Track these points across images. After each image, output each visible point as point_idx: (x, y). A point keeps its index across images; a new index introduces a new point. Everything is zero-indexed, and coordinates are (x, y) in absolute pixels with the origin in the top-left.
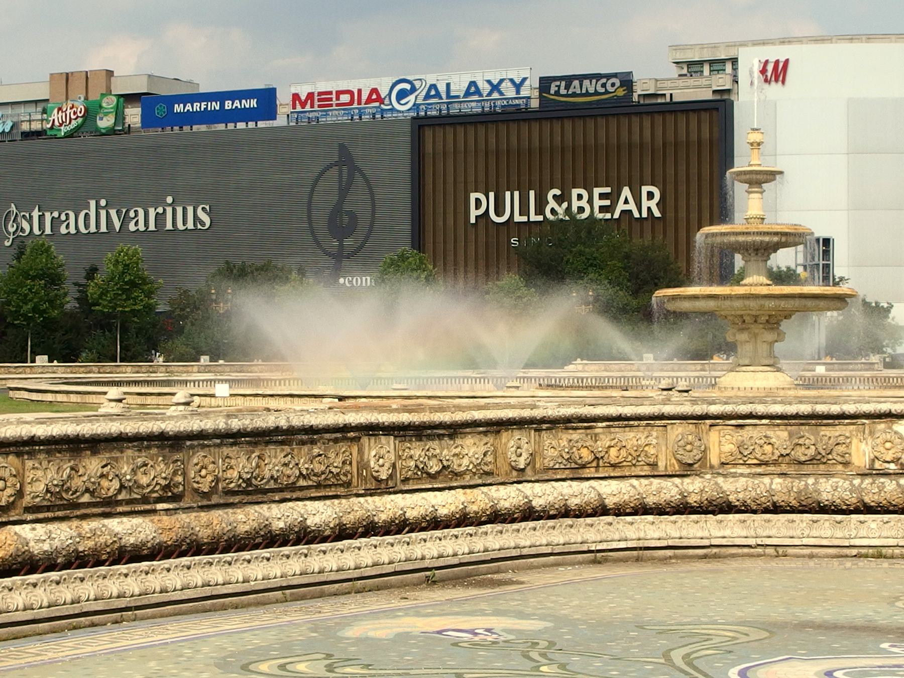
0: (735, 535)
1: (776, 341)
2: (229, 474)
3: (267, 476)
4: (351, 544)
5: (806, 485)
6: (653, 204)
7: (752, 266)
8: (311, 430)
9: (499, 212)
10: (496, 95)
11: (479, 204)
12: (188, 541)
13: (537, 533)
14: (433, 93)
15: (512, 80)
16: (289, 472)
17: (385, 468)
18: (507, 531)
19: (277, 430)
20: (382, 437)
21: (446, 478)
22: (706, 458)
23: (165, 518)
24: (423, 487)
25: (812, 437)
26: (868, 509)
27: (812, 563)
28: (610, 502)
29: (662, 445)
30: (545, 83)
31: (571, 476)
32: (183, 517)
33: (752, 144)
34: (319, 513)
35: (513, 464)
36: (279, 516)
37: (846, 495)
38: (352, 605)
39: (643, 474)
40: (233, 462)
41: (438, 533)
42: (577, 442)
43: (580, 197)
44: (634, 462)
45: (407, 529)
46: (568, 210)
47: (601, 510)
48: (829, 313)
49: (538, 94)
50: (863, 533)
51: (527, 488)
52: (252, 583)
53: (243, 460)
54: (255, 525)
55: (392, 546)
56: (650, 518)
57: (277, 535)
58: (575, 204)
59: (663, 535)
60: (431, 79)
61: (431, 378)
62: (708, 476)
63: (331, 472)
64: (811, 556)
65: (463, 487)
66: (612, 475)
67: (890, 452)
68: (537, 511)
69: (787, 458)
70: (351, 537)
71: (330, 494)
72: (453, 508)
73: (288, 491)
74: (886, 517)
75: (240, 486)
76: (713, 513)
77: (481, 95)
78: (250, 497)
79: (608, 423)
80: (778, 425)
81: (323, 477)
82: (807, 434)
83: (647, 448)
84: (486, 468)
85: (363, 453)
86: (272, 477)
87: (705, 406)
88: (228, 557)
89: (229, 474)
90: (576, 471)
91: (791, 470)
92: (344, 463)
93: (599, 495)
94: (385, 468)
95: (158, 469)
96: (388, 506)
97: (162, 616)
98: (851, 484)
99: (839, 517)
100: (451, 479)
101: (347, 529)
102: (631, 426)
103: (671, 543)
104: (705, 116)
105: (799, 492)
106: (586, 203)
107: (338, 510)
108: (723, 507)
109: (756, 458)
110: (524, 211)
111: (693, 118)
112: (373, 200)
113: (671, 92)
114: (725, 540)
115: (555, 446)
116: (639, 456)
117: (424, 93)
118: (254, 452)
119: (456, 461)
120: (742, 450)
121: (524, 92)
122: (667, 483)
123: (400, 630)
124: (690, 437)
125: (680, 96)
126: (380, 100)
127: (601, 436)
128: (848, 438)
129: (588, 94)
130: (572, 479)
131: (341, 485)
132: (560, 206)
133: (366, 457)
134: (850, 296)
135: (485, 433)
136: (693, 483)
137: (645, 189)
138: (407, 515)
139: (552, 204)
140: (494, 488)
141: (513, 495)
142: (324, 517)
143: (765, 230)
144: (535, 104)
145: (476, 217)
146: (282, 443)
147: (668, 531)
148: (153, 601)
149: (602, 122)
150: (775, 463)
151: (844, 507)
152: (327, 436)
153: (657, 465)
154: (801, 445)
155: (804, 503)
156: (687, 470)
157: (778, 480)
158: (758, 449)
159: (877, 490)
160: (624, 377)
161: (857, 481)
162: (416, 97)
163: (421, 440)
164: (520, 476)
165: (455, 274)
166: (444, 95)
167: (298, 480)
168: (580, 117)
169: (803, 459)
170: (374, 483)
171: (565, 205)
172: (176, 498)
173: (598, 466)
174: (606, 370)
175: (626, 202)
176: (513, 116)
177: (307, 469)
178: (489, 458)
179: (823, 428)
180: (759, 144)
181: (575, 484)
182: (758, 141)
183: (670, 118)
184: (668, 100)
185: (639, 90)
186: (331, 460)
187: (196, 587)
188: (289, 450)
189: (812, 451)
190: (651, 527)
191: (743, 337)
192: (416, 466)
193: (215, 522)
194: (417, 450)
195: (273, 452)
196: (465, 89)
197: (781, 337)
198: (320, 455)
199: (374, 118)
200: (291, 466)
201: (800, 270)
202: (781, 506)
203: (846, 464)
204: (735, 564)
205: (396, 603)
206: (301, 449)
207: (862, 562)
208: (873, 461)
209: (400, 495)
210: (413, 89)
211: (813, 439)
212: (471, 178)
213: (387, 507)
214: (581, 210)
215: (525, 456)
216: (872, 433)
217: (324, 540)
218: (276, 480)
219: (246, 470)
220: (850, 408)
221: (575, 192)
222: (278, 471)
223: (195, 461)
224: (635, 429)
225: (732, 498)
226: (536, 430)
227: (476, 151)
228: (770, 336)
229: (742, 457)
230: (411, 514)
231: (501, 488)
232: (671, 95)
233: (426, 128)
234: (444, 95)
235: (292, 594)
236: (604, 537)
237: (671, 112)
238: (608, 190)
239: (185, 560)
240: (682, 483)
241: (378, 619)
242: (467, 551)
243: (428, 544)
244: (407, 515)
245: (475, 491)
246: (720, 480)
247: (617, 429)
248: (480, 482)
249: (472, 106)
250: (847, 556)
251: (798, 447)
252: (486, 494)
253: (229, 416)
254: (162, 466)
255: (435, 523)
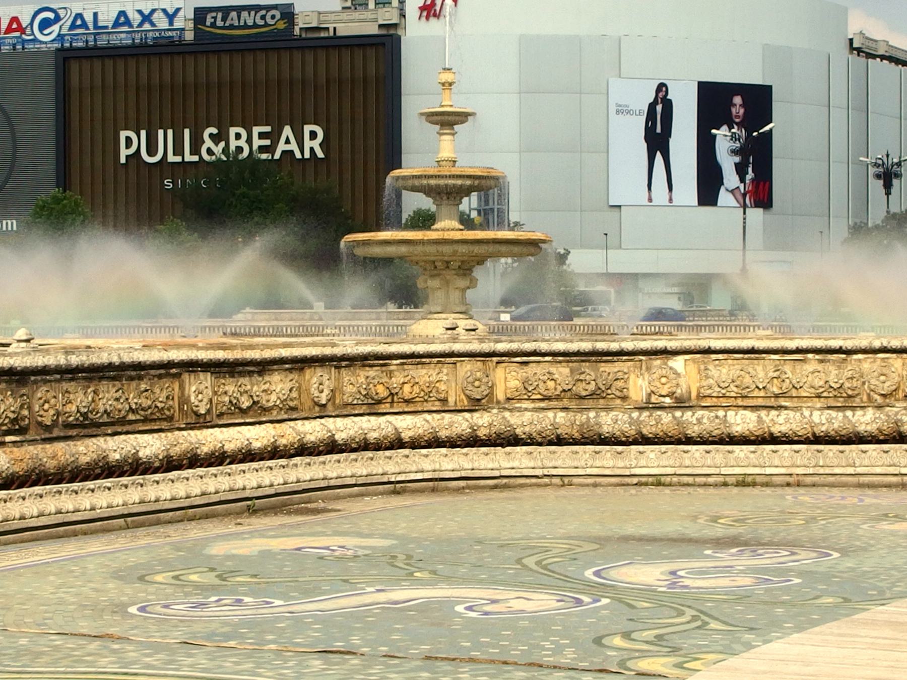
0: (523, 466)
1: (469, 288)
2: (68, 408)
3: (102, 410)
4: (180, 475)
5: (588, 418)
6: (316, 144)
7: (444, 210)
8: (139, 367)
9: (151, 151)
10: (147, 26)
11: (130, 143)
12: (37, 471)
13: (342, 465)
14: (79, 22)
15: (164, 11)
16: (120, 406)
17: (204, 403)
18: (315, 463)
19: (110, 366)
20: (201, 374)
21: (257, 413)
22: (493, 394)
23: (15, 449)
24: (237, 421)
25: (592, 373)
26: (644, 440)
27: (599, 490)
28: (406, 436)
29: (451, 381)
30: (200, 14)
31: (368, 411)
32: (32, 450)
33: (443, 84)
34: (150, 445)
35: (316, 399)
36: (115, 448)
37: (626, 427)
38: (212, 528)
39: (434, 409)
40: (72, 397)
41: (255, 465)
42: (373, 378)
43: (238, 136)
44: (426, 398)
45: (228, 461)
46: (225, 151)
47: (397, 443)
48: (503, 260)
49: (192, 25)
50: (643, 462)
51: (330, 423)
52: (98, 511)
53: (80, 396)
54: (95, 457)
55: (216, 476)
56: (443, 450)
57: (113, 466)
59: (457, 466)
60: (76, 9)
61: (100, 327)
62: (495, 411)
63: (156, 407)
64: (595, 485)
65: (272, 422)
66: (406, 410)
67: (666, 387)
68: (339, 445)
69: (569, 394)
70: (179, 467)
71: (156, 427)
72: (265, 442)
73: (118, 424)
74: (664, 448)
75: (77, 419)
76: (502, 445)
77: (131, 26)
78: (86, 430)
79: (402, 361)
80: (560, 362)
81: (150, 411)
82: (588, 370)
83: (437, 385)
84: (292, 404)
85: (184, 389)
86: (105, 411)
87: (492, 344)
88: (75, 486)
89: (68, 408)
90: (373, 406)
91: (573, 405)
92: (168, 398)
93: (396, 429)
94: (204, 403)
95: (8, 403)
96: (209, 440)
97: (22, 542)
98: (630, 417)
99: (620, 448)
100: (260, 414)
101: (174, 460)
102: (423, 363)
103: (463, 474)
104: (371, 52)
105: (582, 425)
106: (244, 141)
107: (165, 443)
108: (511, 440)
109: (540, 394)
111: (359, 53)
112: (14, 140)
113: (335, 25)
115: (354, 382)
116: (430, 392)
117: (69, 23)
118: (89, 387)
119: (265, 397)
120: (527, 386)
121: (178, 23)
122: (458, 417)
123: (264, 548)
124: (478, 374)
125: (344, 30)
126: (22, 30)
127: (396, 373)
128: (626, 373)
129: (246, 26)
130: (369, 414)
131: (165, 420)
132: (217, 145)
133: (187, 392)
134: (544, 241)
135: (290, 370)
136: (482, 417)
137: (308, 128)
138: (226, 448)
139: (208, 143)
140: (300, 422)
141: (318, 429)
142: (154, 449)
143: (458, 173)
144: (189, 36)
145: (127, 157)
146: (114, 379)
147: (461, 463)
148: (14, 527)
149: (261, 56)
150: (558, 398)
151: (624, 439)
152: (153, 372)
153: (447, 400)
154: (581, 380)
155: (586, 436)
156: (475, 405)
157: (561, 414)
158: (541, 384)
159: (654, 422)
160: (303, 326)
161: (635, 414)
162: (61, 27)
163: (233, 377)
164: (321, 411)
165: (104, 216)
166: (91, 26)
167: (127, 415)
168: (214, 52)
169: (584, 393)
170: (194, 417)
171: (222, 144)
172: (22, 431)
173: (392, 402)
174: (276, 319)
175: (287, 142)
176: (165, 49)
177: (136, 403)
178: (294, 394)
179: (603, 364)
180: (450, 84)
181: (372, 418)
182: (450, 81)
183: (334, 54)
184: (332, 34)
185: (301, 23)
186: (157, 395)
187: (50, 514)
188: (120, 386)
189: (592, 387)
190: (445, 459)
191: (434, 283)
192: (231, 402)
193: (60, 454)
194: (230, 386)
195: (106, 387)
196: (114, 19)
197: (473, 283)
198: (147, 391)
199: (14, 48)
200: (122, 401)
201: (474, 214)
202: (565, 439)
203: (624, 398)
204: (527, 492)
205: (233, 529)
206: (129, 385)
207: (645, 490)
208: (650, 395)
209: (216, 429)
210: (58, 19)
211: (594, 375)
212: (121, 116)
213: (209, 439)
214: (239, 149)
215: (326, 392)
216: (648, 369)
217: (156, 471)
218: (108, 414)
219: (84, 404)
220: (628, 346)
221: (233, 131)
222: (111, 405)
223: (39, 395)
224: (427, 366)
225: (518, 431)
226: (336, 367)
227: (126, 86)
228: (462, 283)
229: (526, 392)
230: (229, 447)
231: (306, 422)
232: (335, 29)
233: (72, 61)
234: (91, 26)
235: (133, 521)
236: (402, 468)
237: (334, 47)
238: (268, 129)
239: (38, 489)
240: (472, 418)
241: (229, 540)
242: (281, 481)
243: (247, 475)
244: (226, 448)
245: (284, 425)
246: (507, 414)
247: (410, 367)
248: (286, 416)
249: (122, 38)
250: (628, 485)
251: (579, 383)
252: (293, 428)
253: (67, 353)
254: (11, 400)
255: (248, 456)
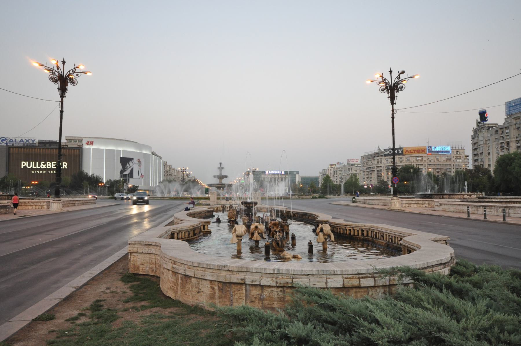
6: (66, 166)
9: (29, 165)
58: (48, 165)
93: (165, 164)
110: (35, 166)
114: (445, 213)
221: (48, 163)
249: (21, 144)
